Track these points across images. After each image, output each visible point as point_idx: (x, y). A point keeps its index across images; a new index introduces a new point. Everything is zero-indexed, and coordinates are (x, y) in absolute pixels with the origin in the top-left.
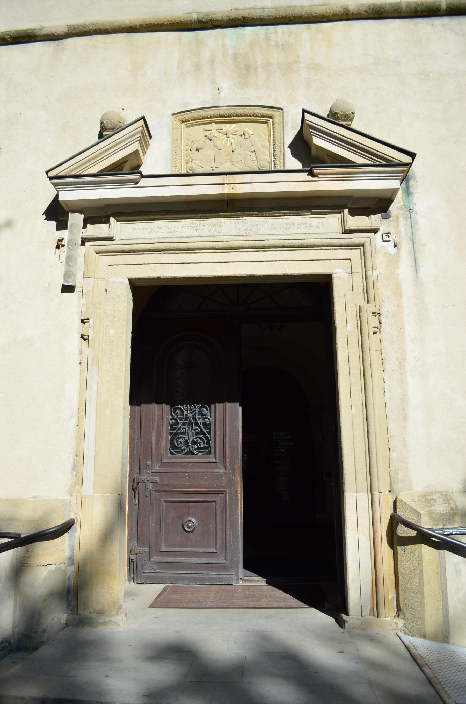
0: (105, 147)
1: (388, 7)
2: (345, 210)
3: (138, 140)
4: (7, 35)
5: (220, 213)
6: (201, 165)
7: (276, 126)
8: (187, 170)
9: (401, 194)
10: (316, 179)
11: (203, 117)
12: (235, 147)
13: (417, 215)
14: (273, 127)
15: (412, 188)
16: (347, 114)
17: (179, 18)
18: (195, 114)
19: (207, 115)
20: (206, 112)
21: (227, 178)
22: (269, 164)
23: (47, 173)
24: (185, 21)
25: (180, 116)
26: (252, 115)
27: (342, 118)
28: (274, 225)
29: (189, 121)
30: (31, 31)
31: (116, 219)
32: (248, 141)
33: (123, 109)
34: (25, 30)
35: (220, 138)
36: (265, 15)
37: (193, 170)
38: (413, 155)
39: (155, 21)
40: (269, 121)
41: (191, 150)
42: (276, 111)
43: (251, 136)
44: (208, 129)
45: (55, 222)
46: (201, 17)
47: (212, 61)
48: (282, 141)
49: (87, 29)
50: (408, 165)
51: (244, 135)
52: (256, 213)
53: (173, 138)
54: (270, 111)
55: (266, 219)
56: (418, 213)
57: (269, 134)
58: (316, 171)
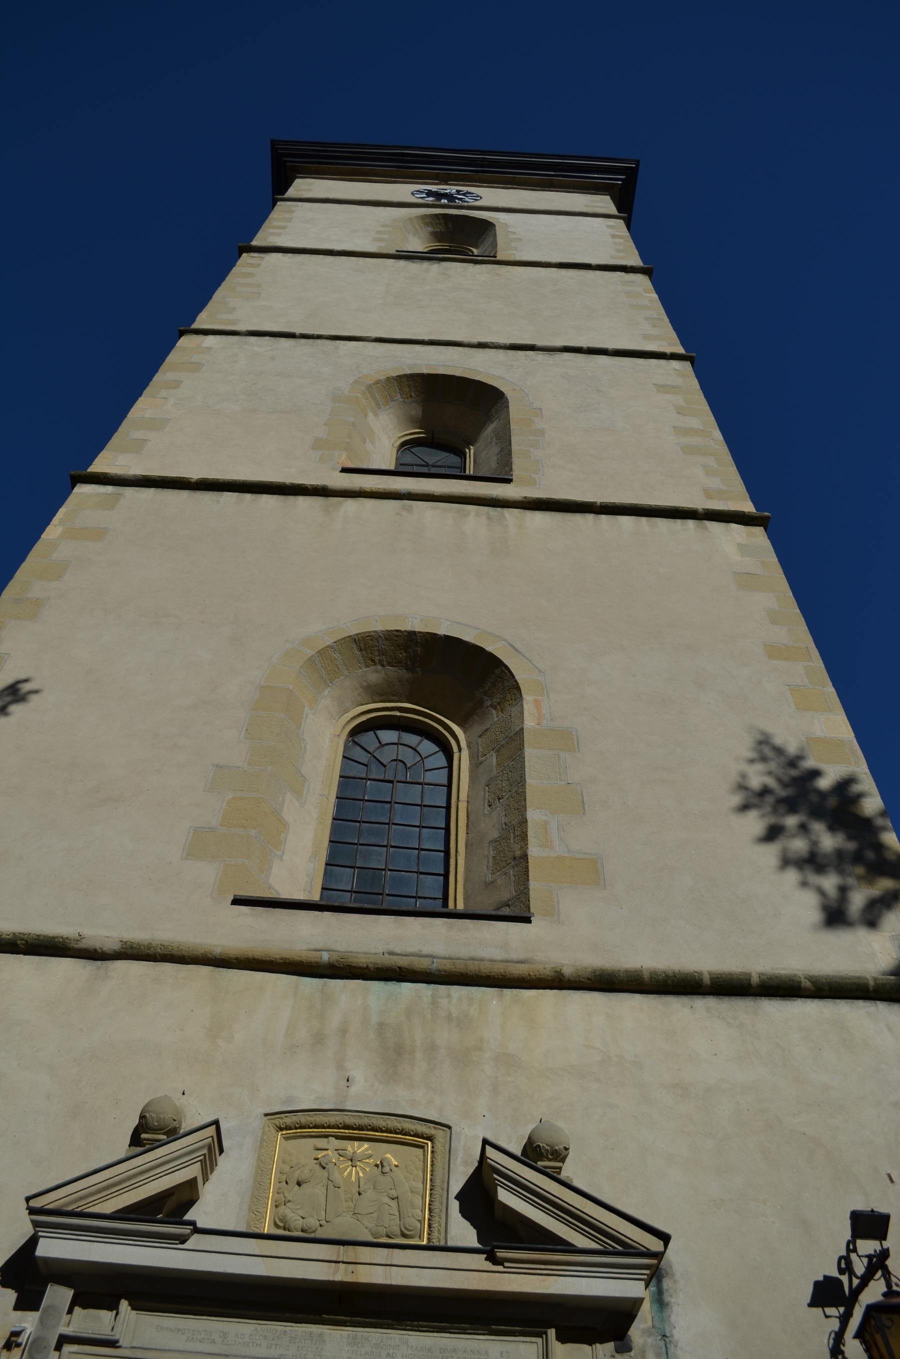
0: (142, 1167)
1: (623, 976)
2: (549, 1331)
3: (201, 1161)
4: (22, 939)
5: (324, 1316)
6: (301, 1213)
7: (438, 1157)
8: (274, 1219)
9: (649, 1305)
10: (500, 1268)
11: (315, 1125)
12: (364, 1187)
13: (678, 1350)
14: (432, 1158)
15: (668, 1293)
16: (556, 1150)
17: (299, 956)
18: (303, 1118)
19: (323, 1123)
20: (322, 1117)
21: (344, 1250)
22: (419, 1224)
23: (28, 1199)
24: (309, 962)
25: (278, 1118)
26: (398, 1131)
27: (547, 1155)
28: (419, 1349)
29: (291, 1129)
30: (61, 940)
31: (130, 1305)
32: (387, 1178)
33: (184, 1094)
34: (52, 936)
35: (341, 1167)
36: (434, 968)
37: (286, 1221)
38: (665, 1238)
39: (262, 956)
40: (426, 1145)
41: (287, 1183)
42: (440, 1129)
43: (394, 1169)
44: (322, 1147)
45: (16, 1292)
46: (334, 957)
47: (343, 1032)
48: (446, 1184)
49: (151, 951)
50: (659, 1256)
51: (382, 1166)
52: (389, 1321)
53: (259, 1157)
54: (430, 1127)
55: (405, 1335)
56: (679, 1345)
57: (424, 1168)
58: (501, 1254)
